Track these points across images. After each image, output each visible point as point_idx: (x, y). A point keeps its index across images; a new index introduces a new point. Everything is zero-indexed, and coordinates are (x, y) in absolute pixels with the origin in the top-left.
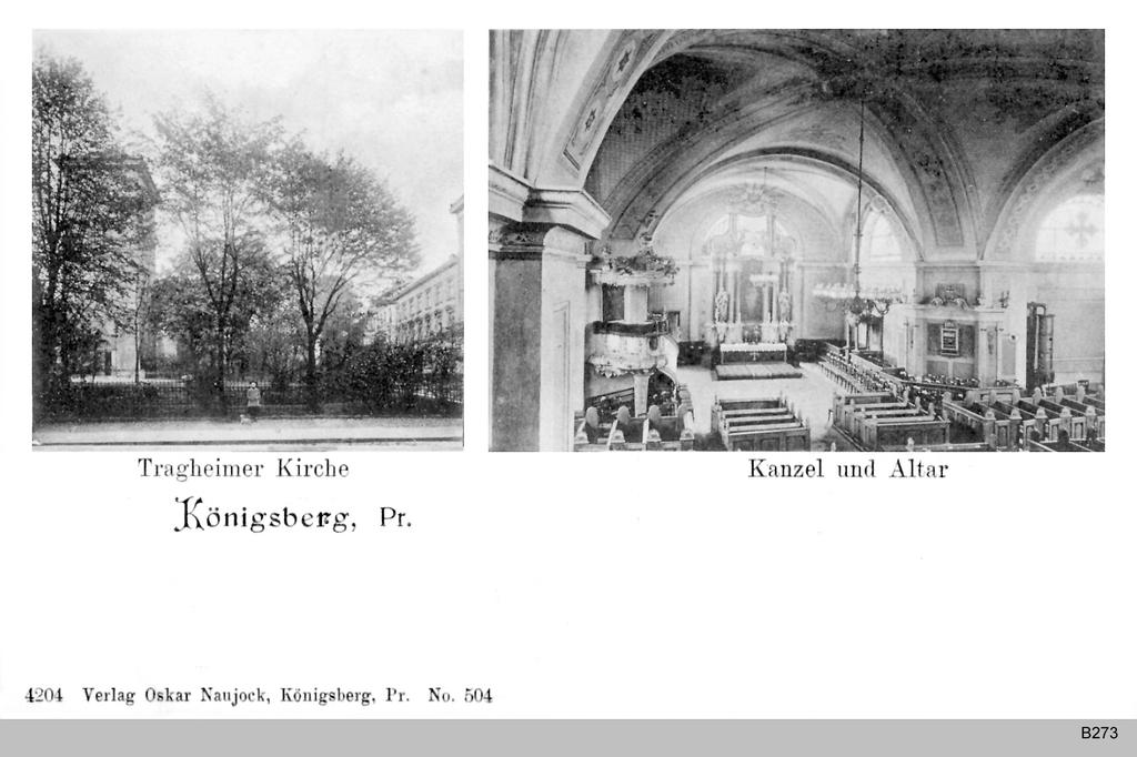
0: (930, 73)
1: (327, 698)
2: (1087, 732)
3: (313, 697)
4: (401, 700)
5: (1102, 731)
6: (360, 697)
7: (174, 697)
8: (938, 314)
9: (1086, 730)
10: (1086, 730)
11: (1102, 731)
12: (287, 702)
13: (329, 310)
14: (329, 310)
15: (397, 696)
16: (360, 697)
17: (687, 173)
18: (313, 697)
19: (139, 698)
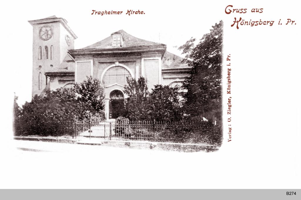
0: (61, 141)
1: (229, 81)
2: (288, 193)
3: (229, 85)
4: (230, 57)
5: (292, 193)
6: (229, 71)
7: (229, 91)
8: (115, 98)
9: (288, 193)
10: (288, 193)
11: (292, 193)
12: (231, 92)
13: (150, 47)
14: (150, 47)
15: (229, 57)
16: (229, 71)
17: (149, 54)
18: (229, 85)
19: (249, 11)
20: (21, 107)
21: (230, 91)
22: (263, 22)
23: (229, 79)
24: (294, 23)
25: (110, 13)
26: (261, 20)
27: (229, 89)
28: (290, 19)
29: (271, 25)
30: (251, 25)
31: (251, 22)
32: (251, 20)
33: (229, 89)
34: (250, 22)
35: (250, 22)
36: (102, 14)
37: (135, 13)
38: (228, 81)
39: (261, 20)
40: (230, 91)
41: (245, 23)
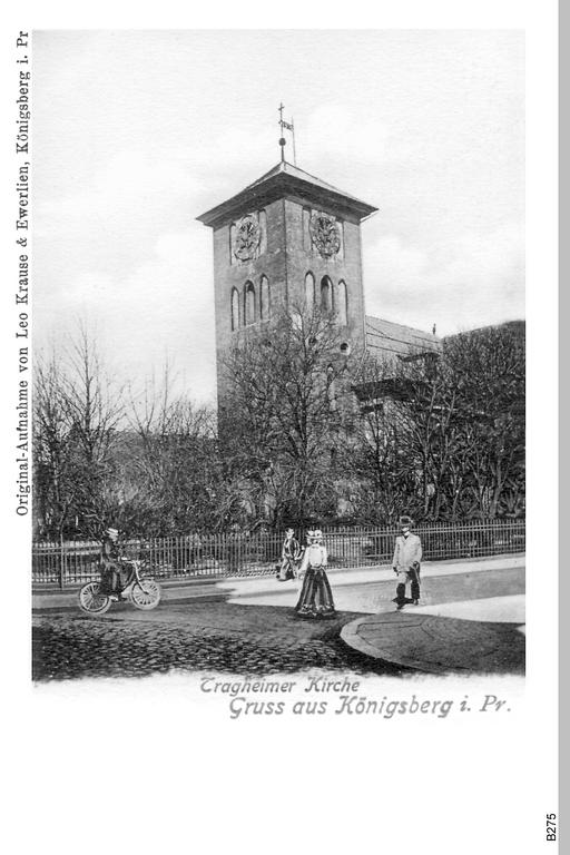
7: (22, 144)
16: (24, 81)
20: (520, 629)
21: (26, 145)
22: (420, 704)
23: (24, 107)
24: (504, 707)
25: (259, 689)
26: (414, 697)
27: (24, 138)
28: (204, 691)
29: (445, 713)
30: (384, 713)
31: (387, 702)
32: (385, 698)
33: (24, 138)
34: (383, 703)
35: (383, 703)
36: (442, 710)
37: (220, 687)
38: (21, 113)
39: (414, 697)
40: (26, 145)
41: (367, 706)
